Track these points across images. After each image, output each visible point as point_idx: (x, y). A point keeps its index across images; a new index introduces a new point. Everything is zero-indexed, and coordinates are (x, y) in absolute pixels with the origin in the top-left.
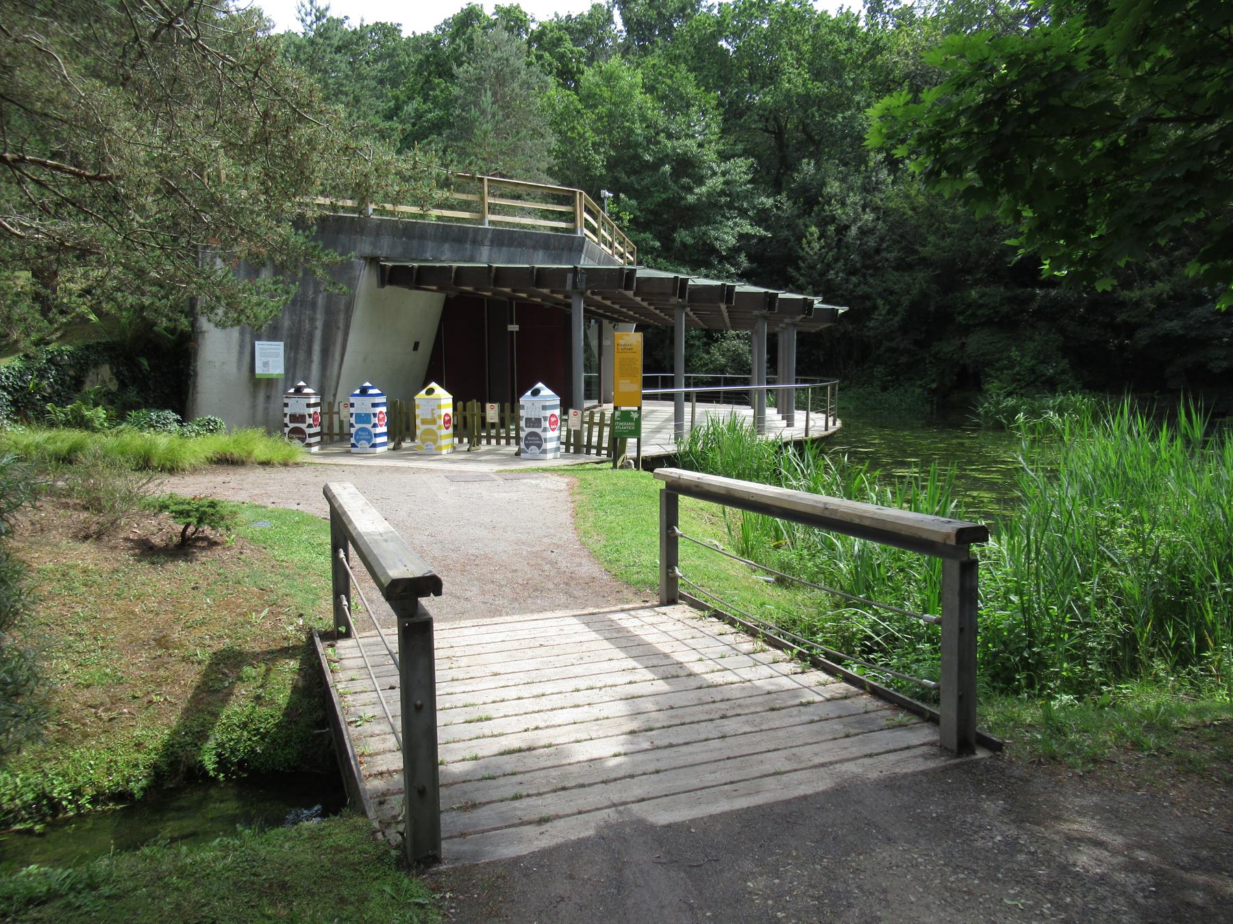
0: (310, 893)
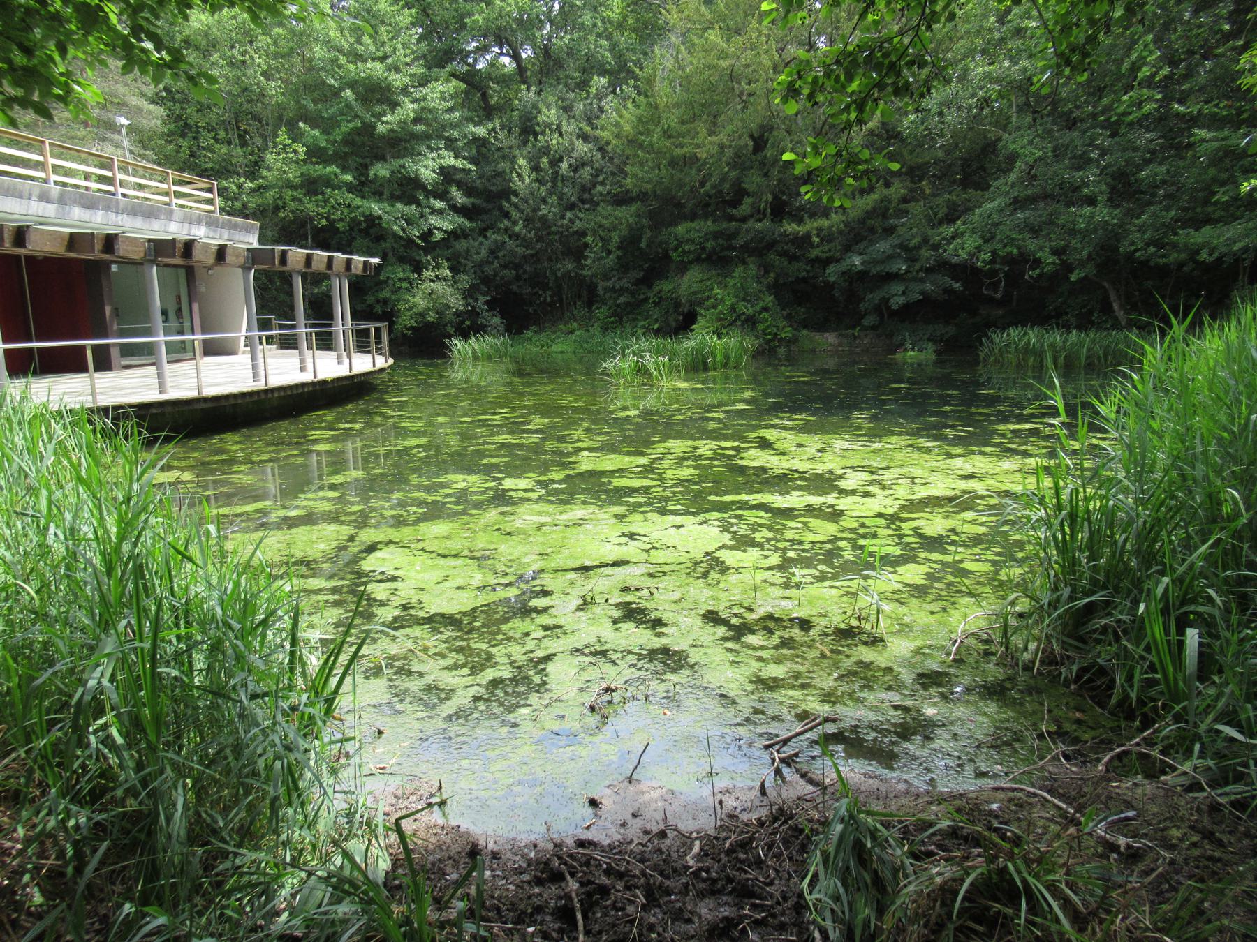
0: (755, 589)
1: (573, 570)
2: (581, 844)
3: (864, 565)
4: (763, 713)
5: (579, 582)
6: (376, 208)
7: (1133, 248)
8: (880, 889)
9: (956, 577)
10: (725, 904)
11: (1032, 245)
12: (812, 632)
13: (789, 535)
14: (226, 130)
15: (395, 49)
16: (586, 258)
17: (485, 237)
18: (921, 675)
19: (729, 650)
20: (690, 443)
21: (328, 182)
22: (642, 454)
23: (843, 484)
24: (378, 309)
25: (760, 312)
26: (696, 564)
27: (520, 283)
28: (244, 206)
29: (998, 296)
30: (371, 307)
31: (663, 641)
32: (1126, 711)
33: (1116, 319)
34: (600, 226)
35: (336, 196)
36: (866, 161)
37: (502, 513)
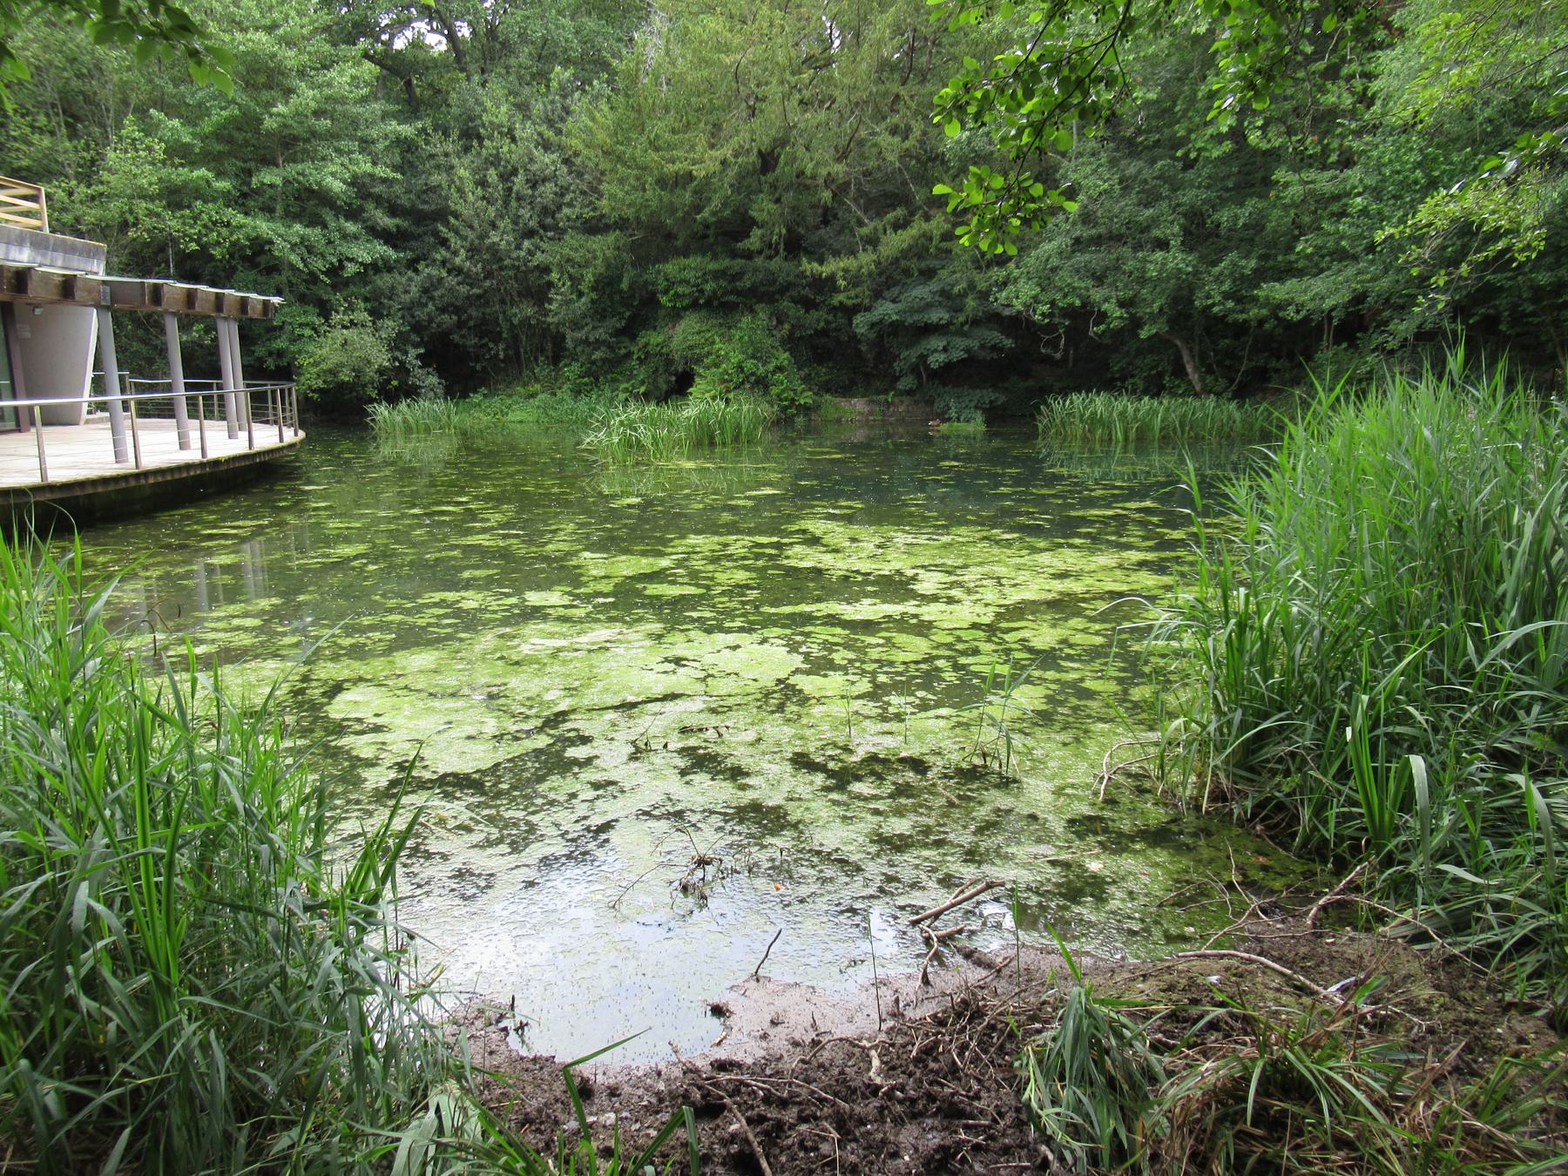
1: (616, 708)
2: (722, 1066)
3: (968, 692)
4: (898, 880)
5: (623, 724)
6: (263, 226)
7: (1210, 302)
8: (1127, 1090)
9: (1080, 699)
10: (932, 1129)
11: (1097, 295)
12: (930, 775)
13: (874, 654)
14: (47, 115)
15: (287, 16)
16: (550, 301)
17: (416, 271)
18: (1072, 822)
19: (835, 803)
20: (716, 539)
21: (201, 193)
22: (662, 554)
23: (919, 588)
24: (270, 363)
25: (774, 373)
26: (768, 695)
27: (464, 331)
28: (77, 220)
29: (1058, 356)
30: (261, 360)
31: (748, 797)
32: (1317, 851)
33: (1190, 383)
34: (568, 260)
35: (210, 211)
36: (1040, 198)
37: (501, 636)
